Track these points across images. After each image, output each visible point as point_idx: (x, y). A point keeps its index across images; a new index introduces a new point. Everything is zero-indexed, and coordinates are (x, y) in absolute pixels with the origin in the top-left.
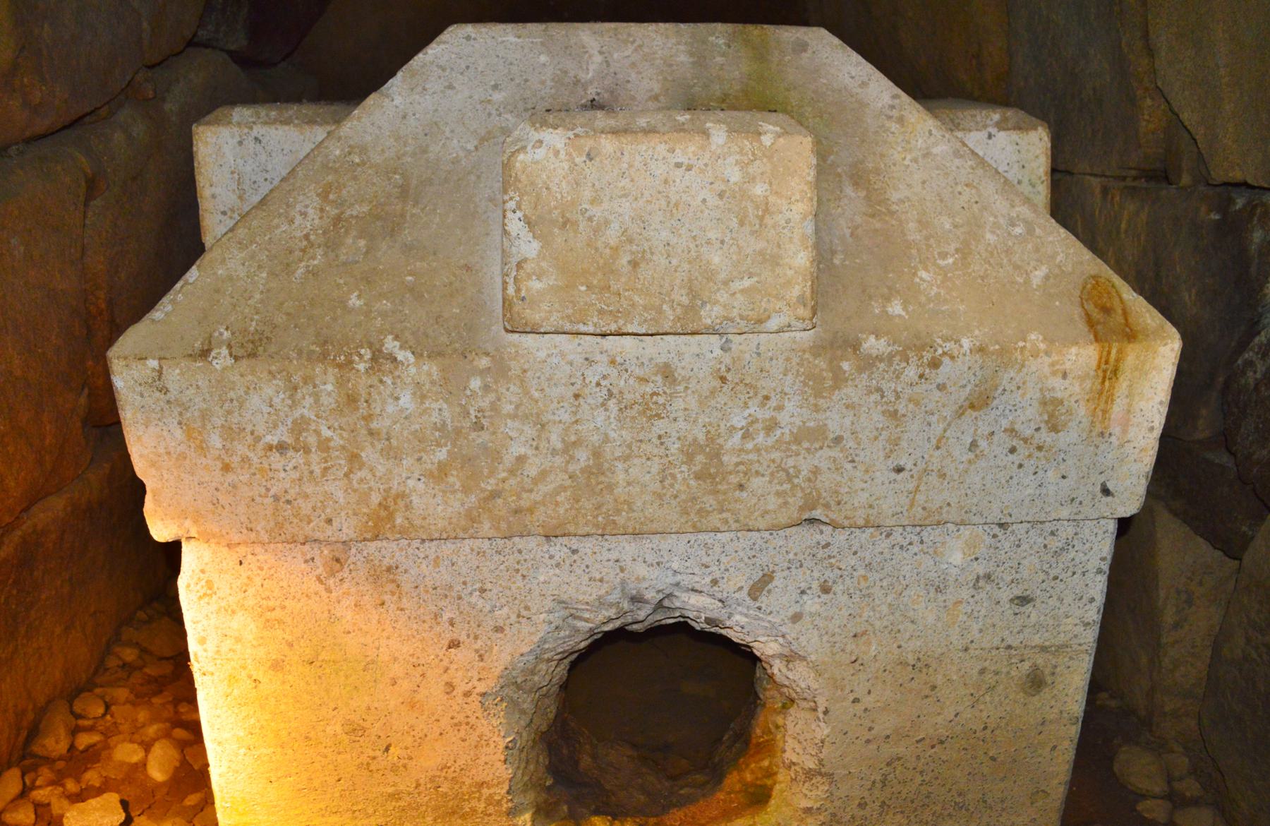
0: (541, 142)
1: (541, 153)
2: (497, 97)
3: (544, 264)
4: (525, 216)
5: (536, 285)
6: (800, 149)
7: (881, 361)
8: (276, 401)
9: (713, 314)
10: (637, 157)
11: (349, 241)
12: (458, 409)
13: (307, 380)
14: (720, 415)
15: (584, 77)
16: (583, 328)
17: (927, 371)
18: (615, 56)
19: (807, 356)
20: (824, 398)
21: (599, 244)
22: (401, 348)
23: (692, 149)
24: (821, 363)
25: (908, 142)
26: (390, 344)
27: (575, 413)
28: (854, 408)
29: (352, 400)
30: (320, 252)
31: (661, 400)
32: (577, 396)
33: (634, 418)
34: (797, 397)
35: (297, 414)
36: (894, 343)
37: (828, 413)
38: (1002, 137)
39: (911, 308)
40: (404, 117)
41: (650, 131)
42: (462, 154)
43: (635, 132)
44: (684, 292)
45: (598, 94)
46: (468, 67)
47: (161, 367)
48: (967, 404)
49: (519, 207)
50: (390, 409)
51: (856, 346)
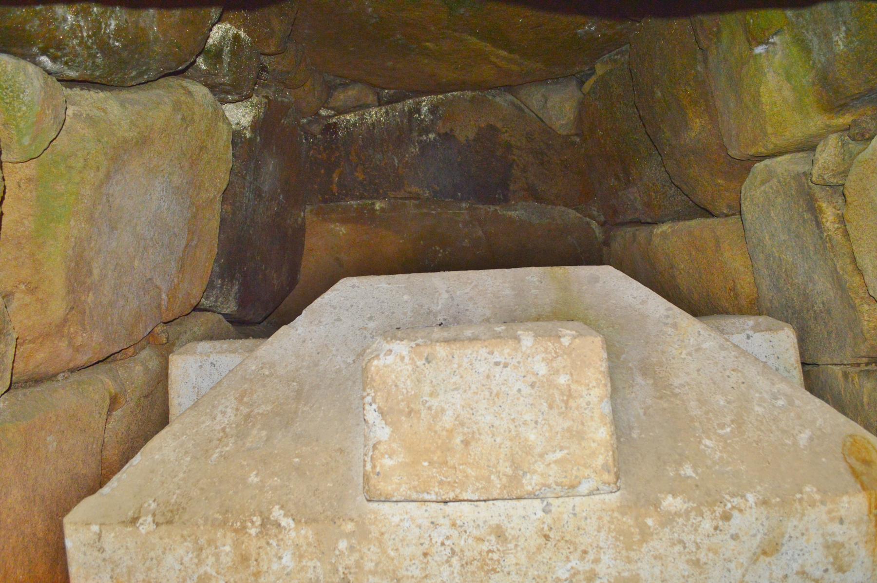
0: (391, 351)
1: (390, 359)
2: (372, 325)
3: (394, 445)
4: (379, 408)
5: (388, 462)
6: (593, 347)
7: (680, 516)
8: (186, 559)
9: (533, 482)
10: (466, 360)
11: (255, 432)
12: (329, 567)
13: (210, 542)
14: (546, 568)
15: (435, 308)
16: (427, 497)
17: (721, 523)
18: (458, 293)
19: (616, 514)
20: (634, 550)
21: (438, 428)
22: (285, 515)
23: (507, 351)
24: (629, 520)
25: (683, 341)
26: (277, 513)
27: (424, 569)
28: (661, 558)
29: (244, 559)
30: (232, 440)
31: (495, 556)
32: (425, 555)
33: (473, 573)
34: (611, 551)
35: (201, 571)
36: (689, 501)
37: (639, 564)
38: (758, 337)
39: (700, 471)
40: (304, 342)
41: (474, 339)
42: (343, 366)
43: (463, 341)
44: (507, 464)
45: (445, 320)
46: (352, 306)
47: (101, 531)
48: (759, 551)
49: (374, 401)
50: (275, 567)
51: (657, 505)
